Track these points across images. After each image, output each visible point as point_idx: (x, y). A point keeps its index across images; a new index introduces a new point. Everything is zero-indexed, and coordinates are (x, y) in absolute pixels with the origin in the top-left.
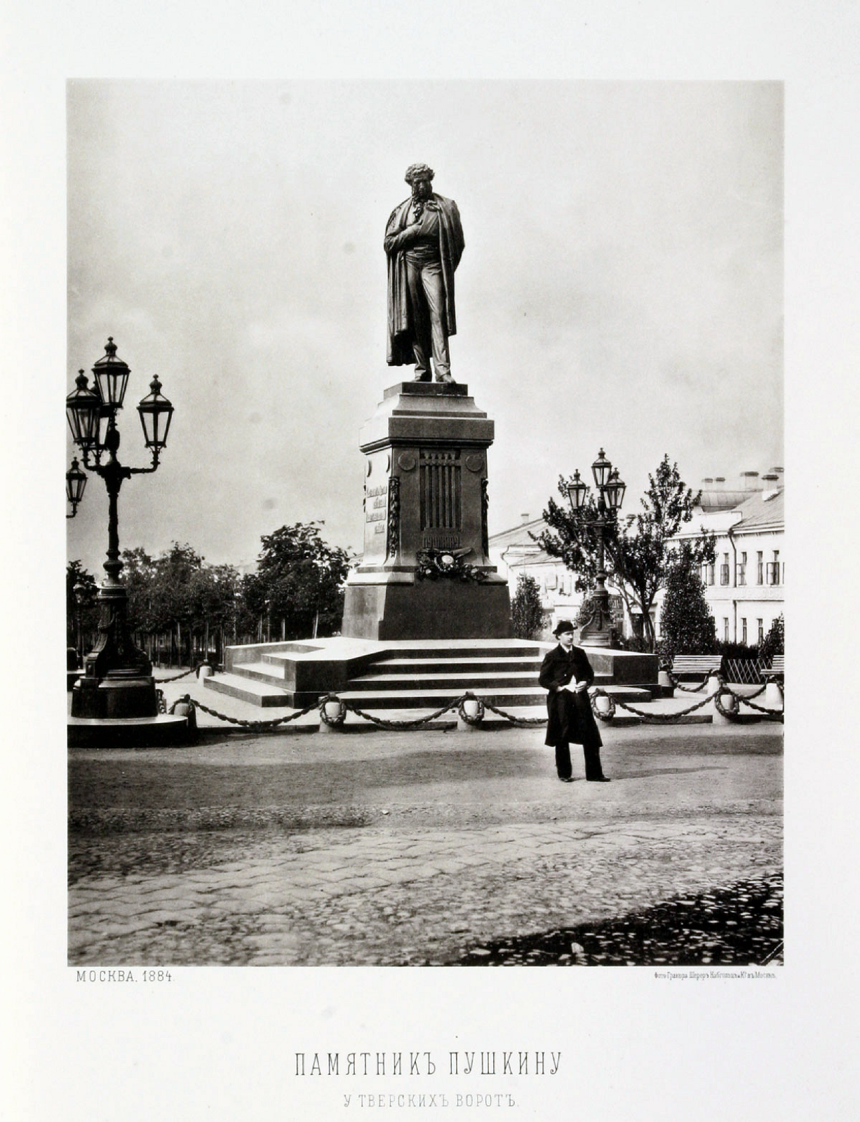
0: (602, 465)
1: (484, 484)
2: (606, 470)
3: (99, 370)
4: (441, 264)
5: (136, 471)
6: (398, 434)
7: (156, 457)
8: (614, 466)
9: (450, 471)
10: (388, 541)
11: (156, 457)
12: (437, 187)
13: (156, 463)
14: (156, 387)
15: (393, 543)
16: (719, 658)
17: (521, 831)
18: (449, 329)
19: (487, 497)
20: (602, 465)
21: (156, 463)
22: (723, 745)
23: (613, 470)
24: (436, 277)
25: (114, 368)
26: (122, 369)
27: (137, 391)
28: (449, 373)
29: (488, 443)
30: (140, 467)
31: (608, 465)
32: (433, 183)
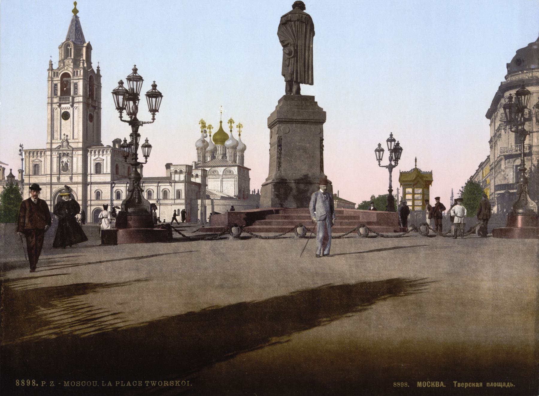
0: (391, 140)
1: (322, 140)
2: (393, 143)
3: (129, 79)
5: (145, 123)
6: (282, 117)
7: (154, 117)
8: (397, 140)
11: (154, 117)
13: (154, 119)
14: (154, 86)
16: (416, 210)
17: (50, 260)
20: (391, 140)
21: (154, 119)
22: (91, 118)
23: (396, 142)
25: (135, 78)
26: (140, 79)
27: (146, 87)
29: (324, 121)
30: (146, 121)
31: (394, 140)
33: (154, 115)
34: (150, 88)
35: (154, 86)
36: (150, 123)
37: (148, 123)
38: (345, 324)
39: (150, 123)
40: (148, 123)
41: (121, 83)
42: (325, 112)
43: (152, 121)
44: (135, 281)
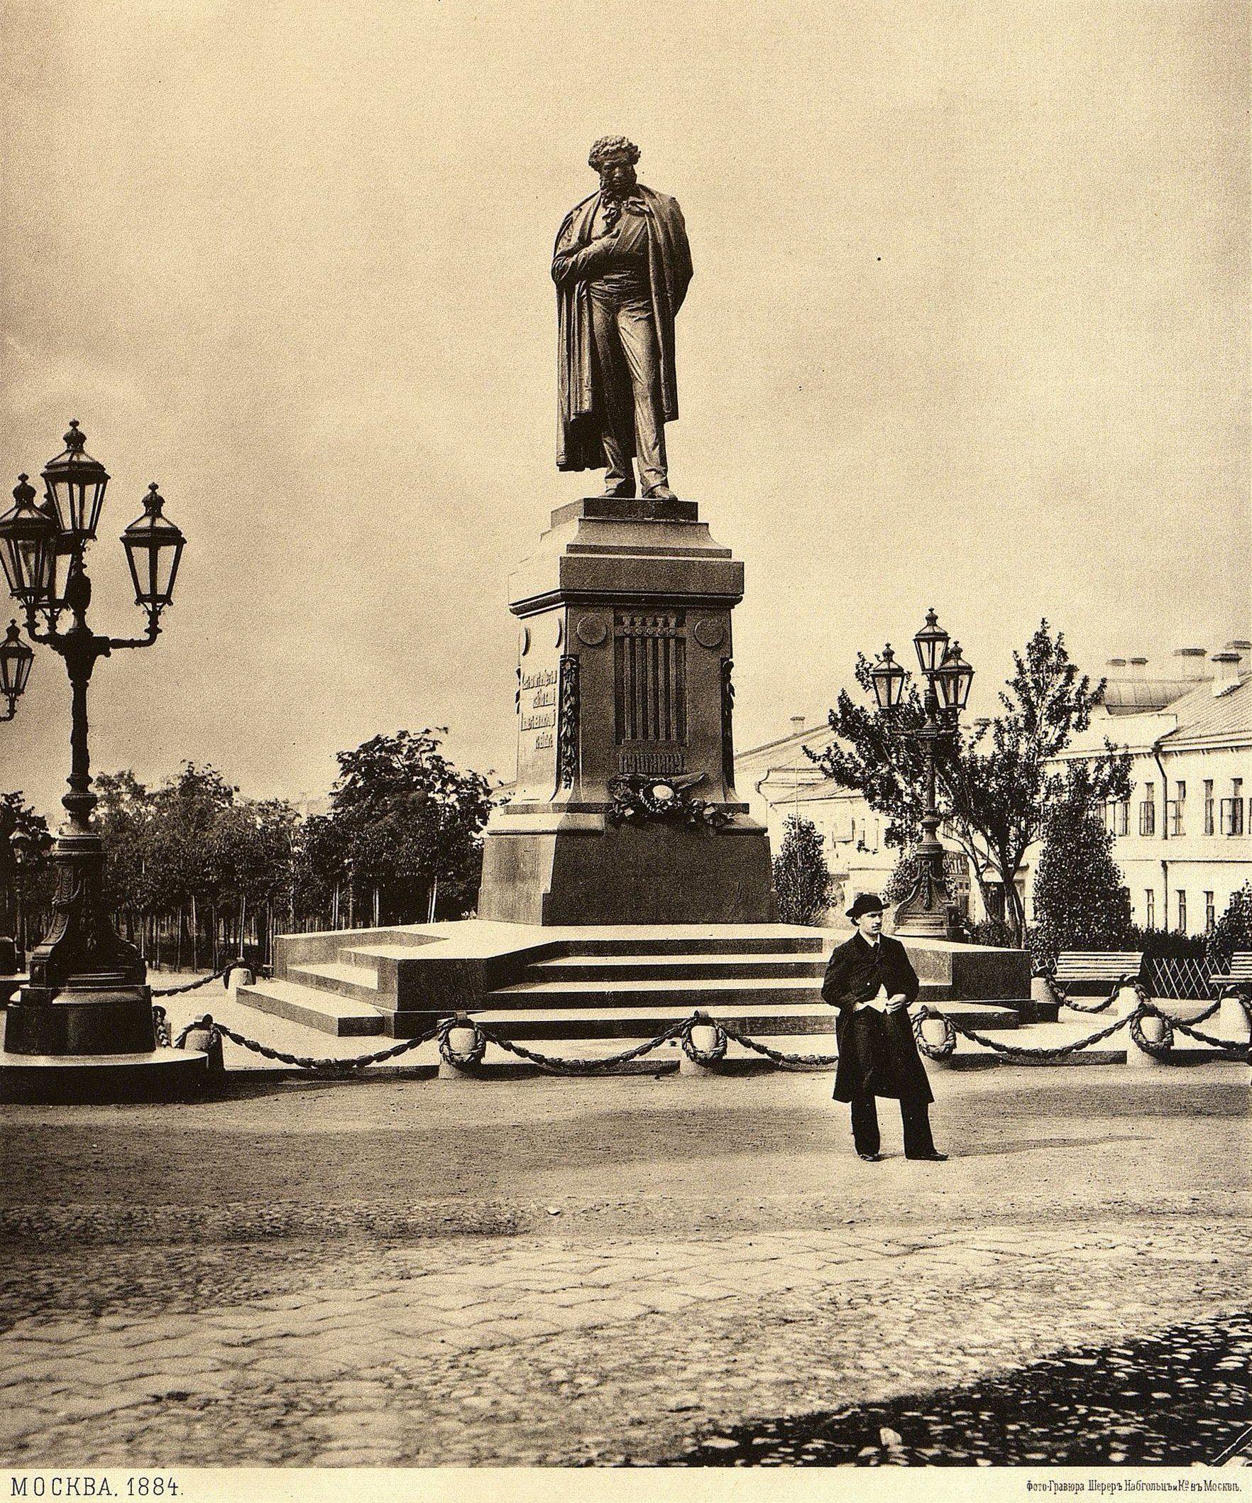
0: (931, 636)
2: (940, 645)
3: (53, 475)
4: (651, 303)
5: (119, 644)
7: (12, 705)
9: (667, 646)
10: (559, 761)
11: (12, 705)
12: (645, 173)
14: (154, 504)
15: (569, 764)
18: (666, 410)
19: (732, 689)
20: (931, 636)
21: (154, 631)
24: (643, 324)
25: (82, 473)
26: (95, 474)
27: (120, 511)
28: (665, 484)
31: (944, 637)
32: (638, 168)
33: (12, 701)
34: (135, 513)
35: (154, 504)
36: (141, 644)
37: (132, 644)
38: (771, 1406)
39: (141, 644)
40: (132, 644)
41: (24, 494)
42: (349, 763)
43: (147, 637)
44: (299, 1336)
